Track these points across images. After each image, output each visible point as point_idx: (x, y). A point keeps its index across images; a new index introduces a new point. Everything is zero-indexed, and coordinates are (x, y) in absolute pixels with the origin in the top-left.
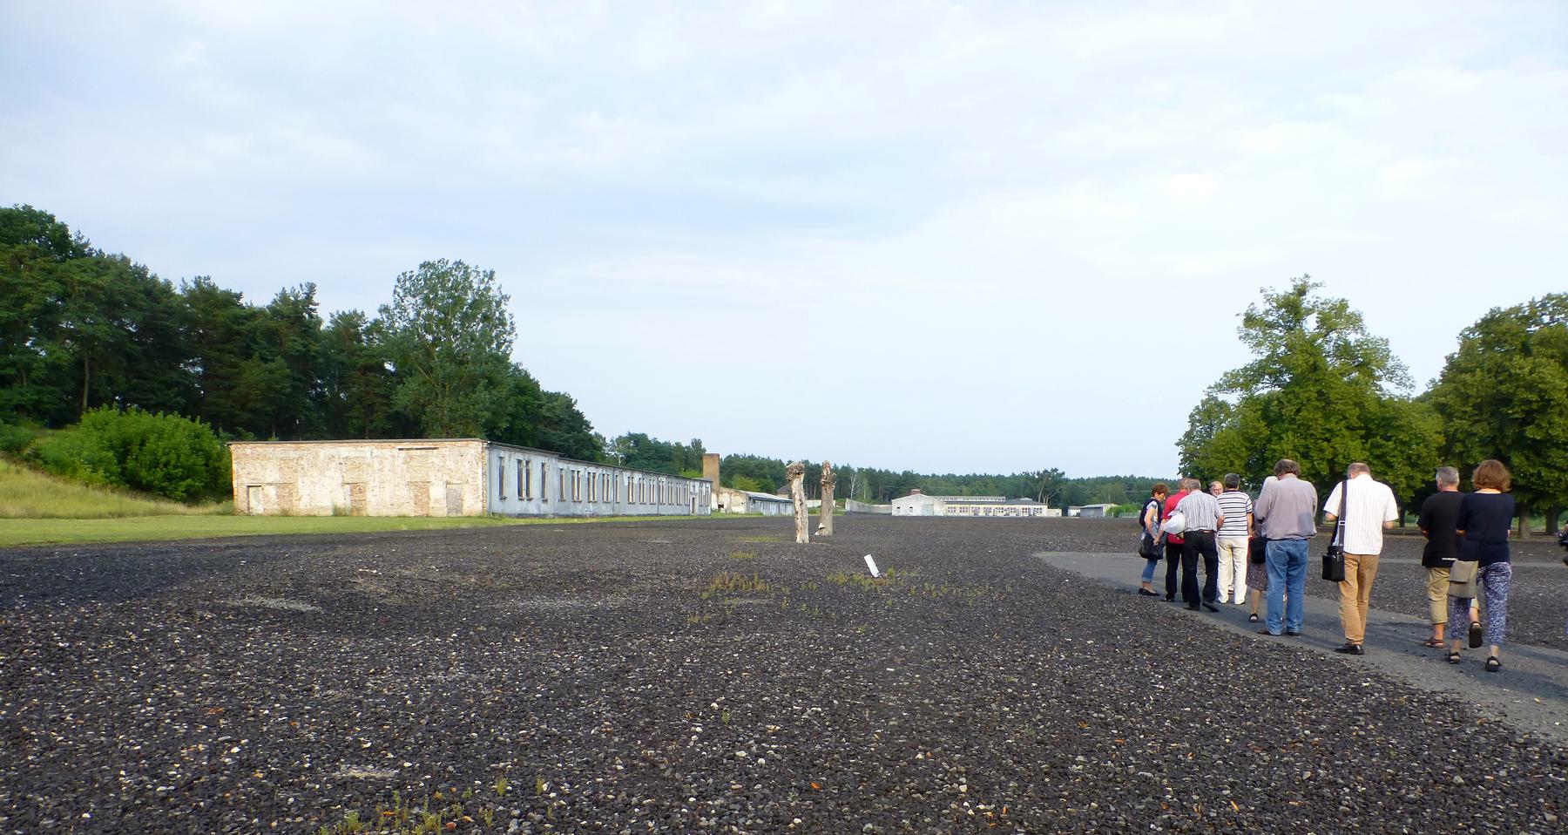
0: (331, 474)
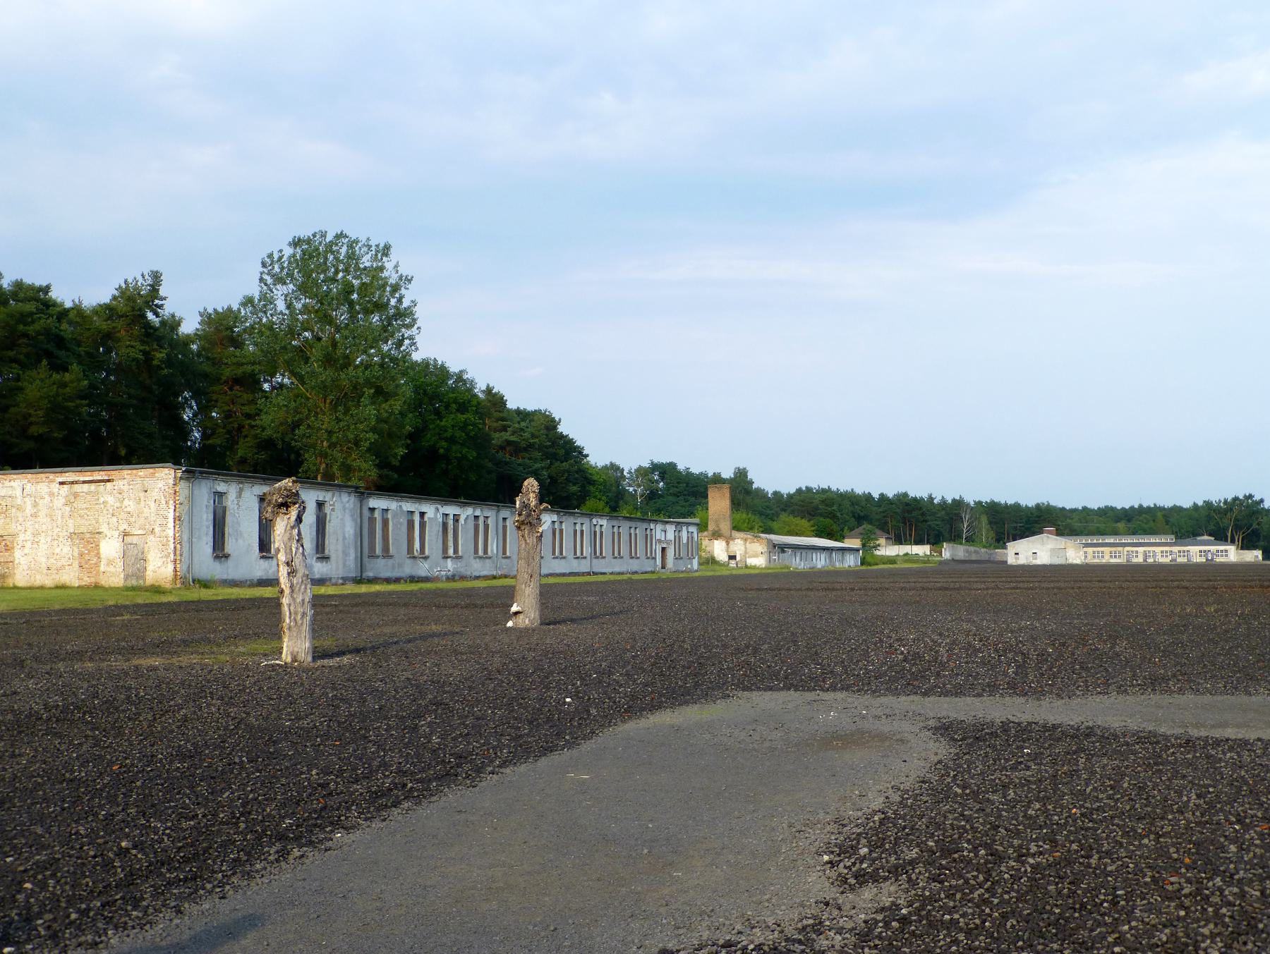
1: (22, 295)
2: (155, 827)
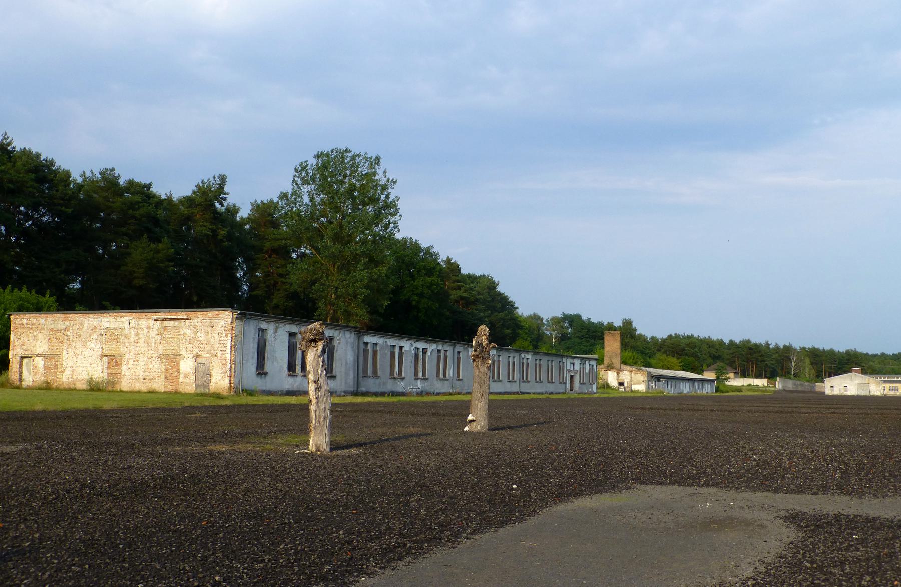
0: (92, 345)
1: (132, 190)
2: (236, 567)
